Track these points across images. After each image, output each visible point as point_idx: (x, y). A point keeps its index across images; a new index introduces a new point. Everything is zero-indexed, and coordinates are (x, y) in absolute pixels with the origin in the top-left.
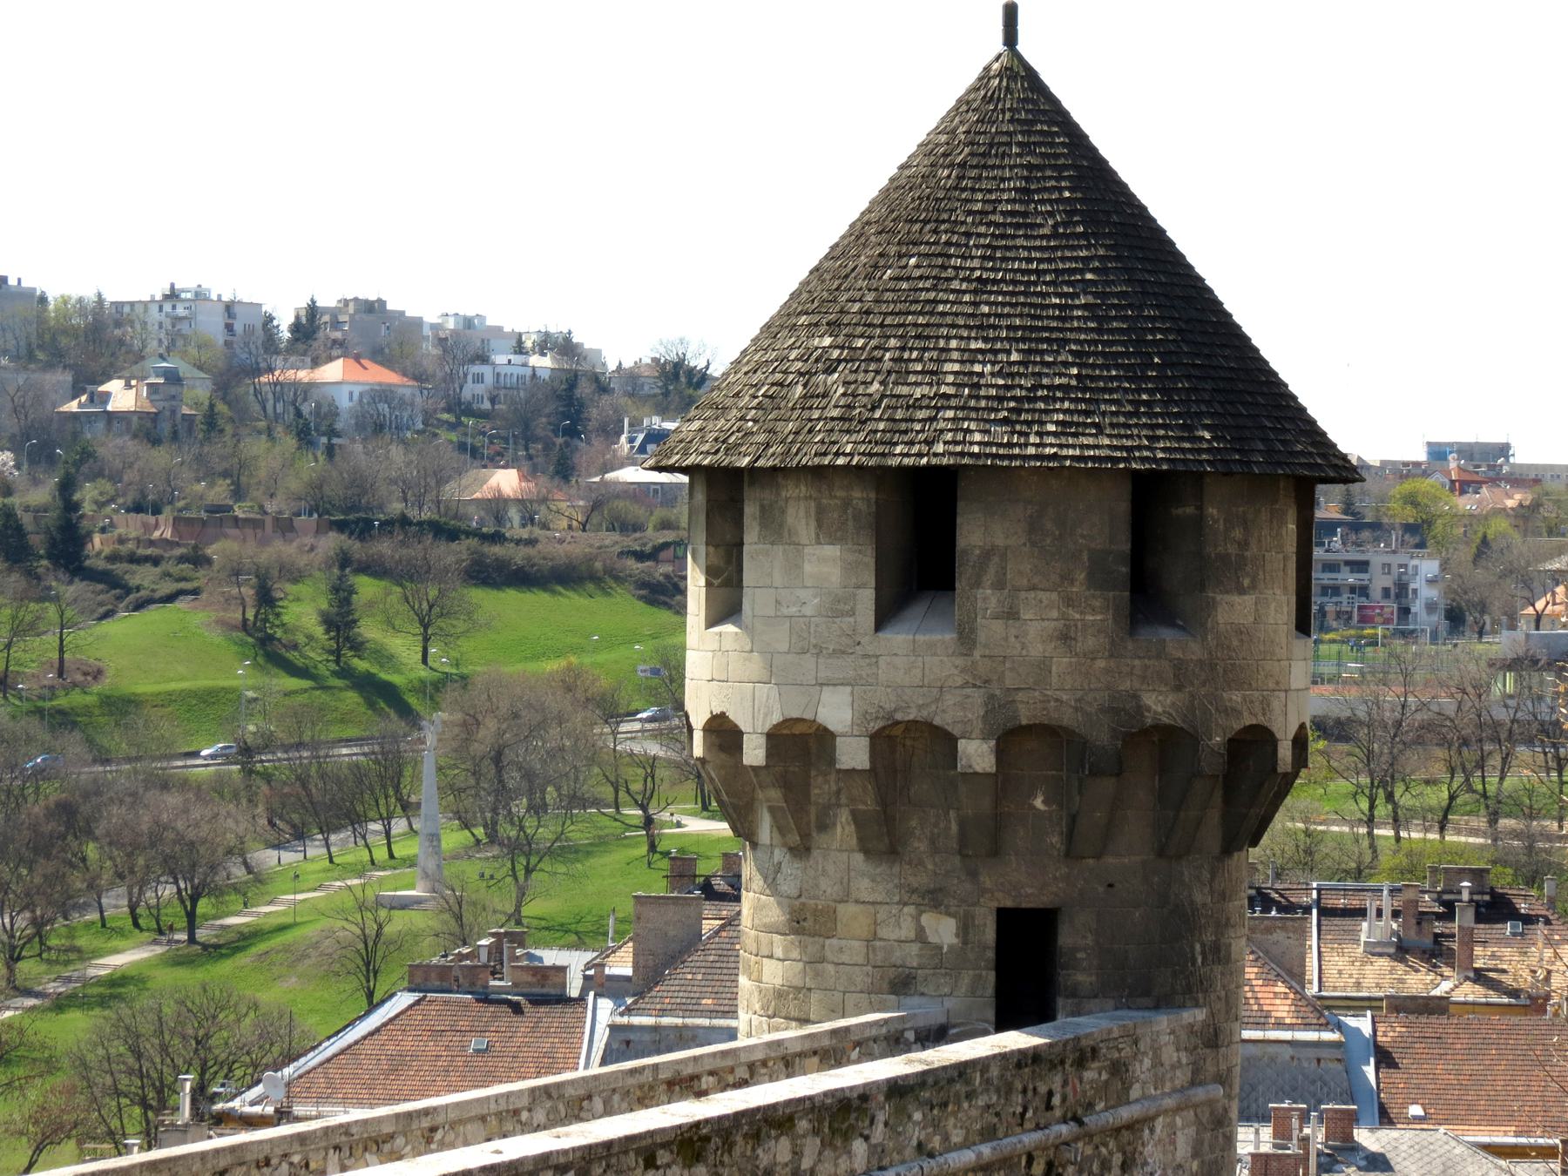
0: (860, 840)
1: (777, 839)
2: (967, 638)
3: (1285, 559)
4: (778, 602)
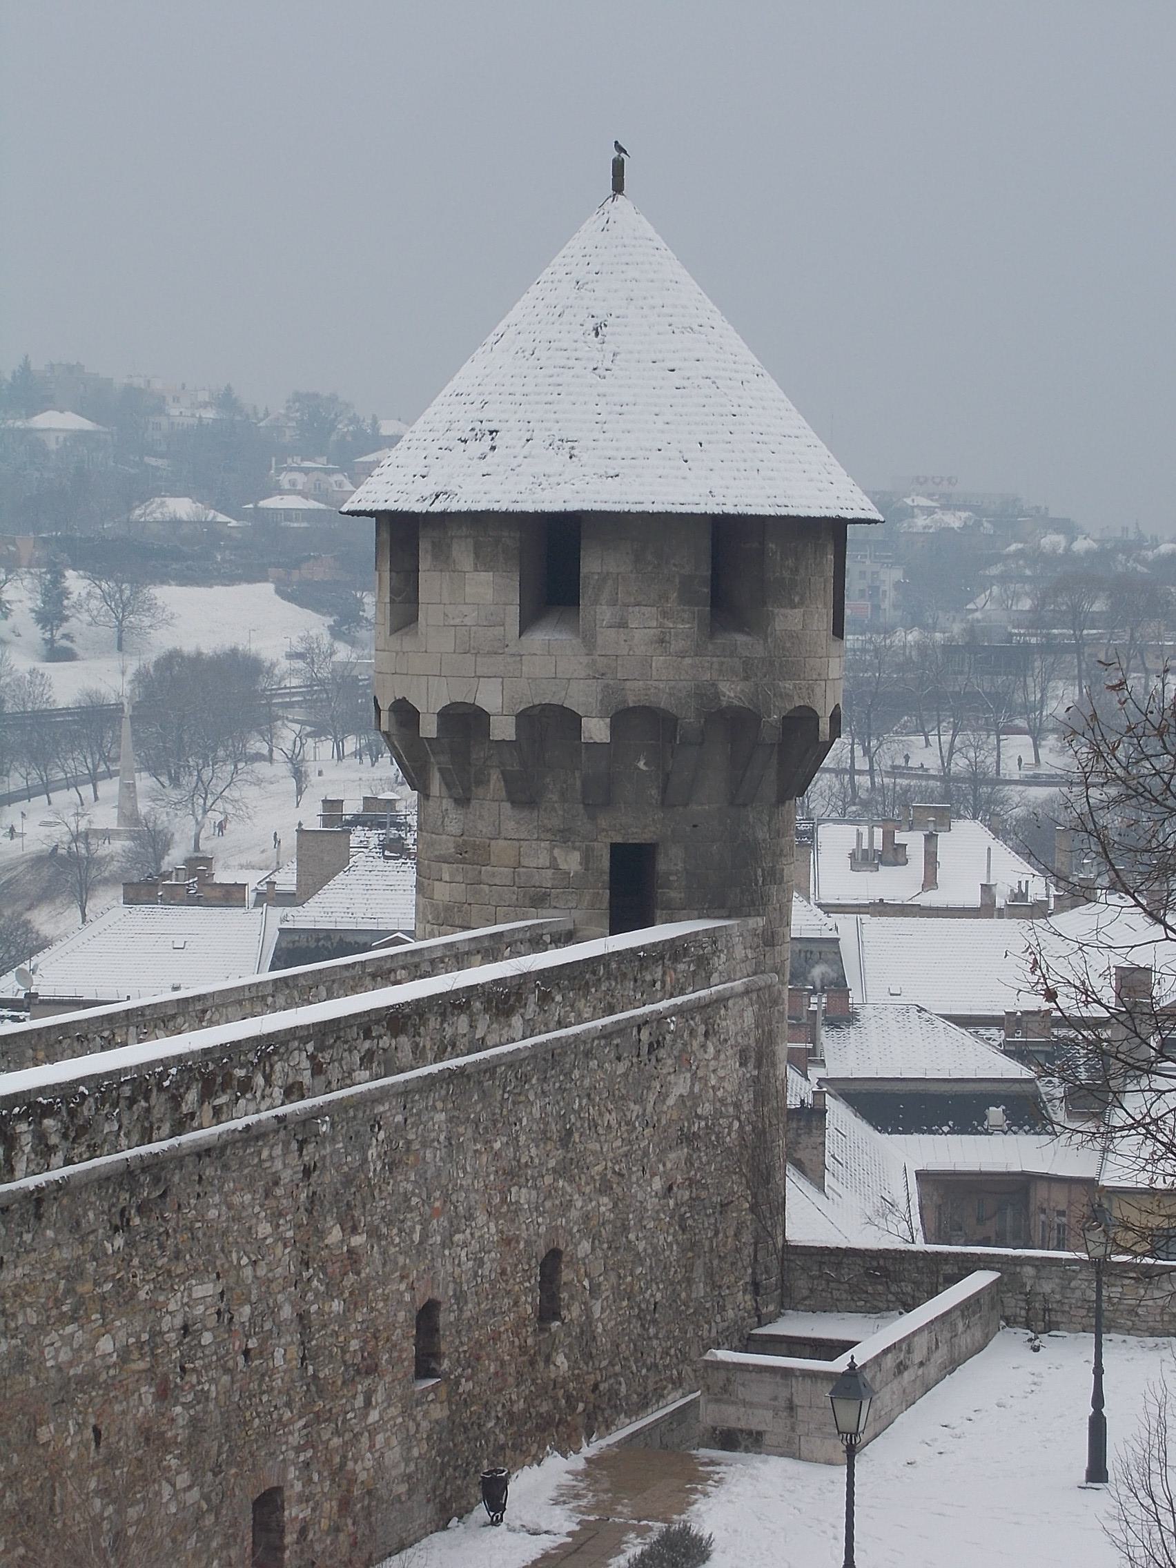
0: (509, 793)
1: (445, 793)
2: (589, 642)
3: (825, 582)
4: (446, 615)
